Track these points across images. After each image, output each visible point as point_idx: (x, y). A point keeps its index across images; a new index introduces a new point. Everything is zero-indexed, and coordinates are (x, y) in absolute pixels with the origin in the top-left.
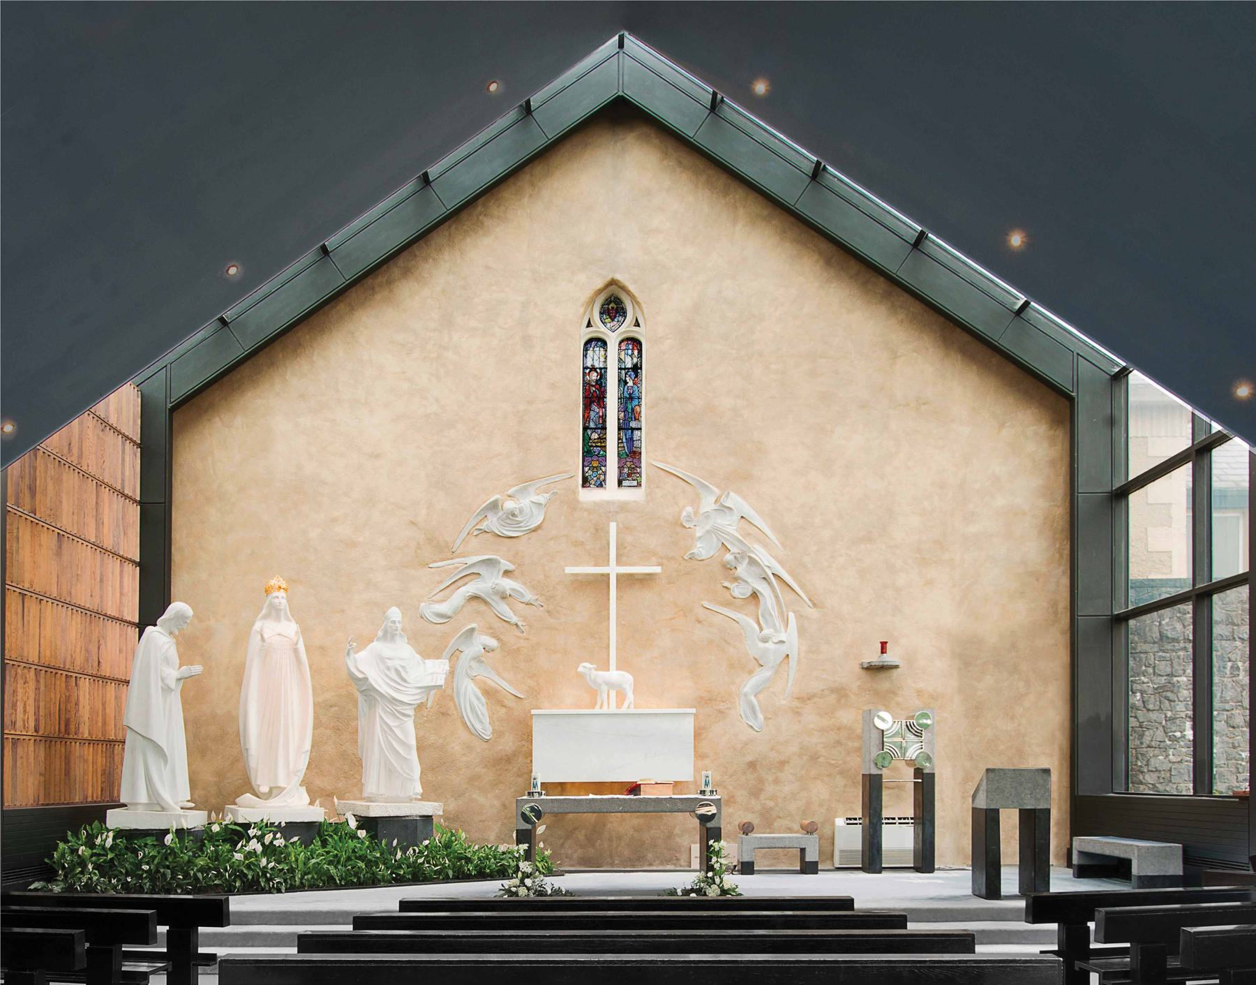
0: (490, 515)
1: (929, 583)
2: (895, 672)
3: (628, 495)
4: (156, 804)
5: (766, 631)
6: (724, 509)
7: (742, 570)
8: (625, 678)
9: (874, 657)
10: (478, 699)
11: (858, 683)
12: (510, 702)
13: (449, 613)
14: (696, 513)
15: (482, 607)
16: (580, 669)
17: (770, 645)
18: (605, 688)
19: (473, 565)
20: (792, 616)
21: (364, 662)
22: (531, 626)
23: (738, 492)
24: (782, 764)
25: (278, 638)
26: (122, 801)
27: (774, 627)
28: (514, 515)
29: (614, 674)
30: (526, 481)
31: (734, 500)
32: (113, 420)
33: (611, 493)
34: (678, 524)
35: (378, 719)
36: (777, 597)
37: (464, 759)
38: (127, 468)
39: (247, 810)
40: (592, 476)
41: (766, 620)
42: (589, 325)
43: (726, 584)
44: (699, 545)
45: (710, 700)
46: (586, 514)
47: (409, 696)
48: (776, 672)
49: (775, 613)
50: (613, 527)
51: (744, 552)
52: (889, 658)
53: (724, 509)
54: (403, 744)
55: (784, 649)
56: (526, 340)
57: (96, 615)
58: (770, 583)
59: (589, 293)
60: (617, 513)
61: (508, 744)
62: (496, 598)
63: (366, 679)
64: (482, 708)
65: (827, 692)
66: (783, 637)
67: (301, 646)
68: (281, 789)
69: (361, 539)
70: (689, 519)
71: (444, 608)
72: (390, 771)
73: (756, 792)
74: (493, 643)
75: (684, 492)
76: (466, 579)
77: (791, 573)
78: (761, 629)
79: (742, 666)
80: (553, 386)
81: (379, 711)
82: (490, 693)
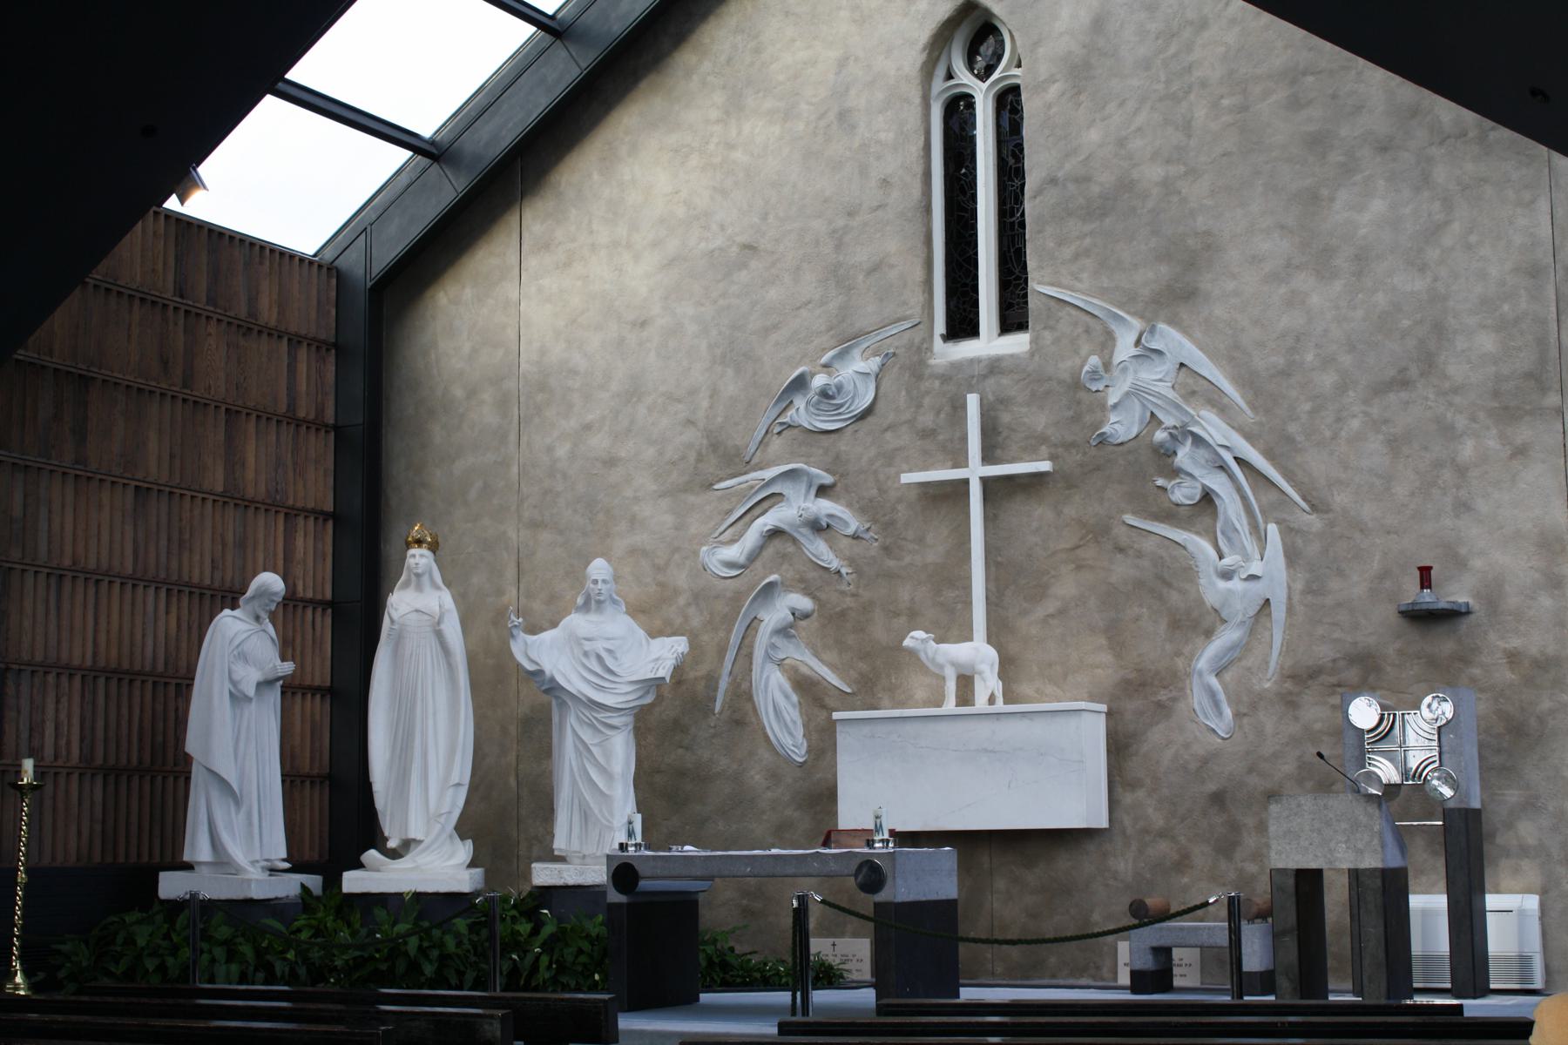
1: (1521, 452)
2: (1464, 625)
3: (1017, 343)
4: (222, 861)
7: (1184, 456)
9: (1411, 593)
10: (787, 697)
11: (1397, 645)
14: (1107, 366)
15: (790, 548)
16: (907, 642)
17: (1236, 584)
21: (547, 651)
22: (858, 572)
23: (1173, 322)
25: (414, 616)
26: (186, 858)
30: (847, 341)
31: (1170, 339)
32: (268, 313)
33: (990, 343)
34: (1076, 385)
37: (769, 794)
38: (312, 384)
39: (371, 877)
40: (962, 324)
41: (1229, 540)
43: (1160, 482)
44: (1113, 418)
45: (1143, 685)
48: (1252, 632)
49: (1242, 525)
50: (973, 401)
52: (1455, 593)
54: (604, 771)
58: (1232, 477)
60: (985, 377)
62: (805, 531)
63: (541, 672)
64: (792, 714)
65: (1342, 663)
66: (1256, 568)
70: (1094, 375)
71: (735, 552)
72: (586, 816)
73: (1226, 847)
74: (804, 603)
76: (765, 505)
77: (1269, 454)
79: (1195, 622)
80: (885, 183)
81: (571, 720)
82: (807, 687)
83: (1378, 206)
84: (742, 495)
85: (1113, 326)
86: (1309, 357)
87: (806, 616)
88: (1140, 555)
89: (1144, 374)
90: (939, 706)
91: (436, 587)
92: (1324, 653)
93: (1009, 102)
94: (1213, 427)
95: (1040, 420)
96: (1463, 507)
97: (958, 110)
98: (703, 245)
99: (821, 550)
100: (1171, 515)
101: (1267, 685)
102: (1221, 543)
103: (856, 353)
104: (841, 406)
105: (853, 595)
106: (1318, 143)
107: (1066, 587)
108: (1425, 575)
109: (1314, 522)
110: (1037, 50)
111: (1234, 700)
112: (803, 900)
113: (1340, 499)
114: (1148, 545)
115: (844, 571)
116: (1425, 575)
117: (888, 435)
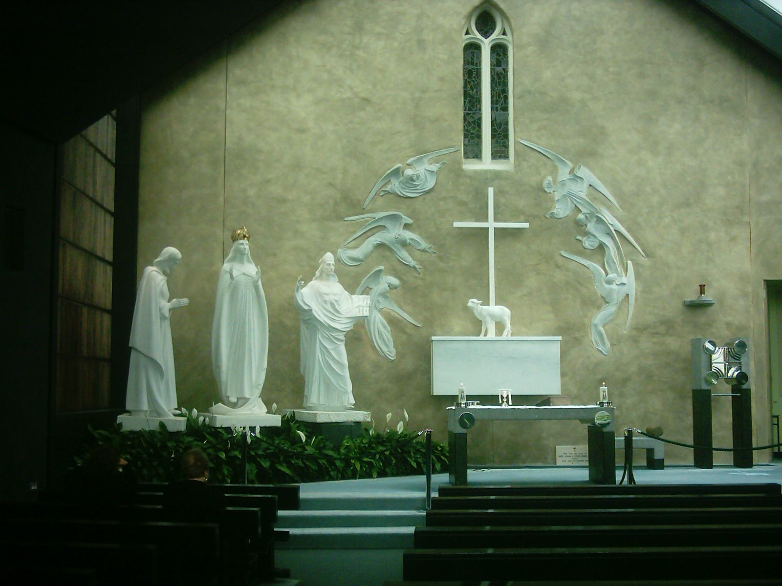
0: (393, 180)
1: (733, 239)
2: (710, 310)
3: (500, 166)
5: (611, 276)
6: (576, 178)
7: (591, 227)
8: (503, 312)
9: (692, 296)
10: (385, 327)
12: (410, 330)
13: (361, 257)
14: (555, 181)
15: (388, 253)
16: (470, 304)
17: (614, 286)
18: (488, 319)
19: (381, 219)
20: (630, 263)
23: (587, 165)
24: (626, 380)
25: (243, 277)
27: (616, 271)
28: (412, 180)
29: (495, 309)
30: (421, 152)
33: (487, 163)
35: (318, 342)
36: (618, 248)
41: (610, 266)
42: (467, 33)
43: (579, 238)
44: (557, 206)
46: (468, 181)
47: (343, 325)
48: (619, 308)
49: (617, 260)
50: (491, 190)
51: (593, 213)
52: (707, 297)
53: (576, 178)
55: (624, 289)
56: (421, 43)
57: (91, 255)
59: (468, 8)
61: (409, 364)
62: (399, 246)
64: (387, 334)
66: (624, 280)
67: (260, 283)
68: (246, 400)
69: (290, 197)
71: (357, 253)
72: (328, 385)
74: (395, 281)
75: (545, 165)
76: (374, 231)
77: (629, 230)
78: (607, 274)
79: (595, 302)
80: (442, 79)
81: (319, 336)
83: (677, 126)
84: (361, 225)
85: (557, 164)
86: (648, 189)
87: (396, 288)
88: (568, 270)
89: (572, 187)
90: (501, 336)
91: (249, 262)
92: (650, 319)
93: (499, 50)
94: (608, 217)
95: (521, 203)
96: (710, 260)
97: (472, 49)
98: (339, 95)
99: (404, 254)
100: (582, 252)
101: (625, 332)
102: (607, 268)
103: (425, 160)
104: (418, 185)
105: (422, 279)
106: (652, 95)
107: (532, 281)
108: (702, 289)
109: (645, 261)
110: (522, 29)
111: (610, 338)
112: (630, 432)
113: (660, 252)
114: (572, 266)
115: (417, 267)
116: (702, 289)
117: (442, 203)
